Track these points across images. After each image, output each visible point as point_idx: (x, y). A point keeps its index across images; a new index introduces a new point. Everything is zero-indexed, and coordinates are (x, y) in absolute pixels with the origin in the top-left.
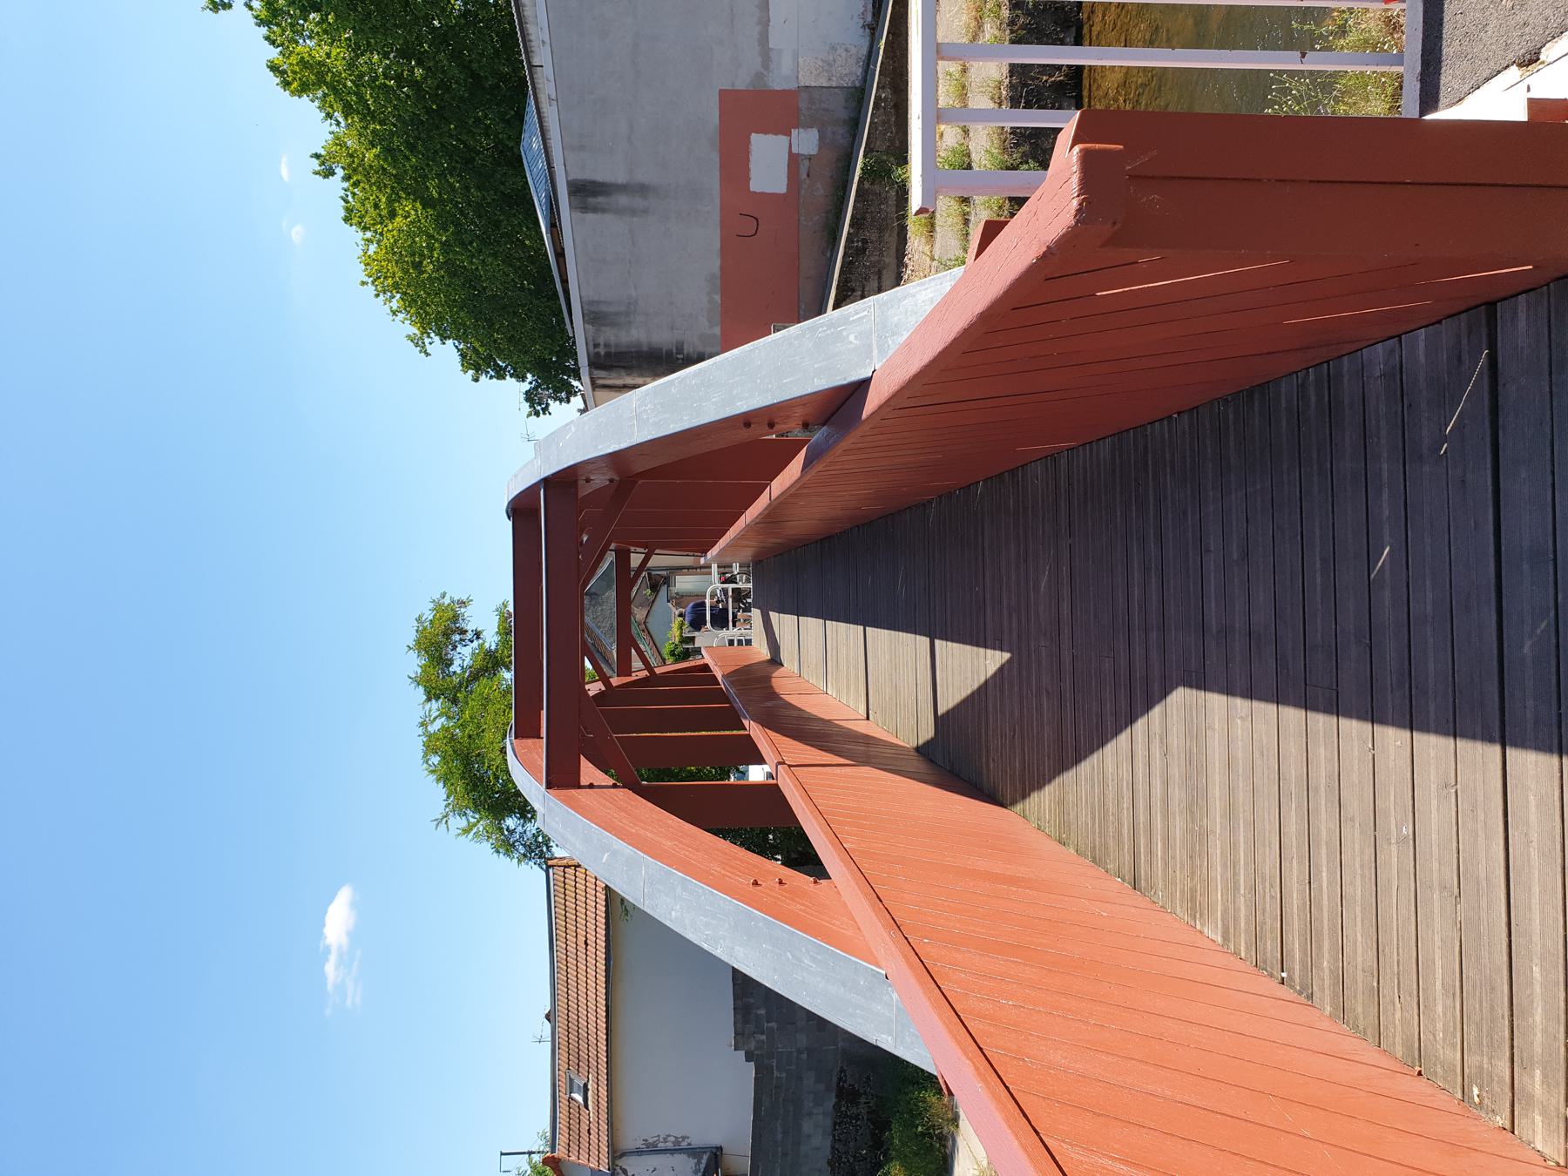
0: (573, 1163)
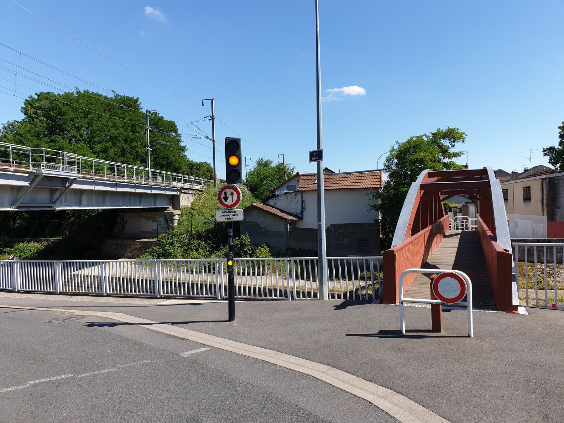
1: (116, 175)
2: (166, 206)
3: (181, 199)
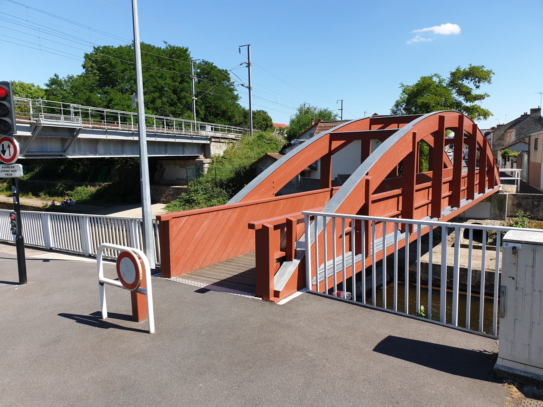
0: (316, 128)
1: (132, 124)
2: (197, 154)
3: (212, 148)
